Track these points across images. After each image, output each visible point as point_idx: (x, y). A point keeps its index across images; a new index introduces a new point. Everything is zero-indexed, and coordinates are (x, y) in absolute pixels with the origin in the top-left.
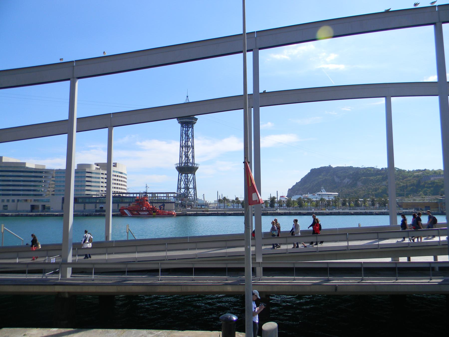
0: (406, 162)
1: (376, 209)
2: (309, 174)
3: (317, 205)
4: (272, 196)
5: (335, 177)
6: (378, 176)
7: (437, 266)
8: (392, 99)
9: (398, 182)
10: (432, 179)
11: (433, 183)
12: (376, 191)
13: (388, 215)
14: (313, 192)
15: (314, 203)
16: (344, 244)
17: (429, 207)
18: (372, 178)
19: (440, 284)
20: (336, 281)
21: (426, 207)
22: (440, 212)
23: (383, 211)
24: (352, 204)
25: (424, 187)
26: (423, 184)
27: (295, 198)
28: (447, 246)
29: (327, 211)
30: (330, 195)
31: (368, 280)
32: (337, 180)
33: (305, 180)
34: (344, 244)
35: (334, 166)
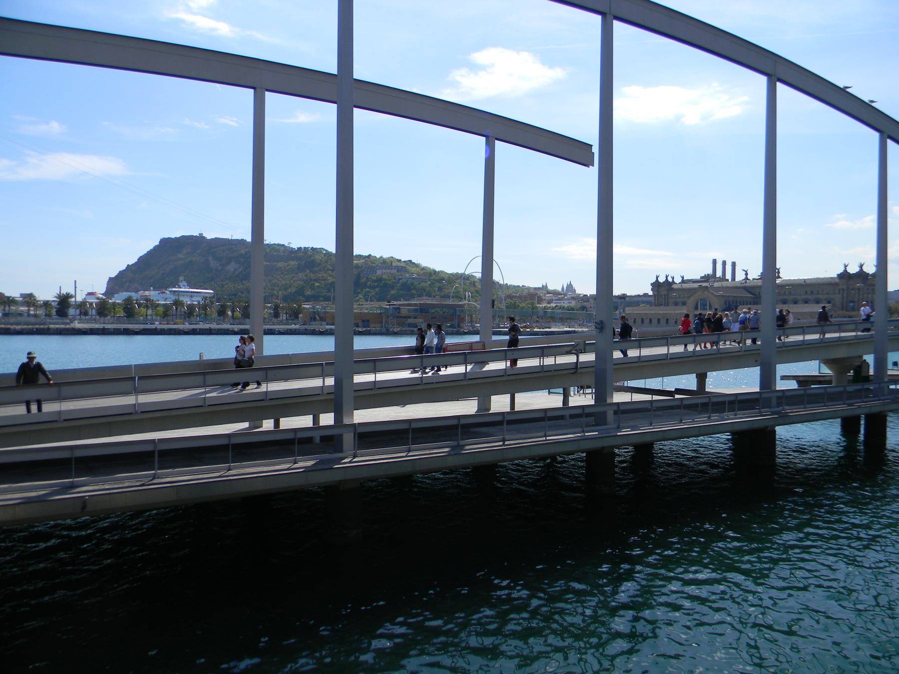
0: (515, 270)
1: (281, 323)
2: (155, 248)
3: (166, 313)
4: (64, 292)
5: (210, 258)
6: (292, 263)
7: (317, 435)
8: (268, 94)
9: (325, 275)
10: (379, 272)
11: (379, 280)
12: (286, 290)
13: (478, 334)
14: (161, 286)
15: (161, 309)
16: (129, 400)
17: (368, 321)
18: (280, 265)
19: (308, 470)
20: (91, 488)
21: (363, 321)
22: (384, 330)
23: (293, 327)
24: (238, 314)
25: (365, 286)
26: (363, 280)
27: (118, 299)
28: (332, 397)
29: (187, 326)
30: (192, 294)
31: (167, 476)
32: (213, 264)
33: (145, 262)
34: (129, 400)
35: (209, 236)
